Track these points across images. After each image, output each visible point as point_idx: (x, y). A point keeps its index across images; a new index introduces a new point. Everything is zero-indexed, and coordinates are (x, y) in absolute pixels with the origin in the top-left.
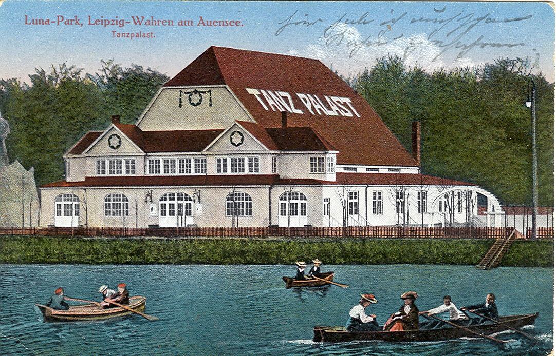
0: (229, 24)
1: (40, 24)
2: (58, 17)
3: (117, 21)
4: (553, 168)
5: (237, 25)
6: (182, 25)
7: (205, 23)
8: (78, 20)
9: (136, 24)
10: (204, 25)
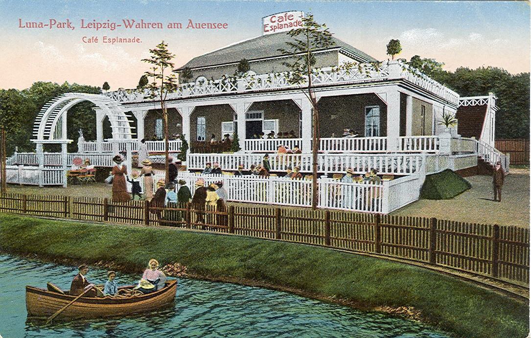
2: (51, 20)
3: (108, 24)
6: (139, 27)
7: (194, 26)
8: (70, 23)
9: (127, 27)
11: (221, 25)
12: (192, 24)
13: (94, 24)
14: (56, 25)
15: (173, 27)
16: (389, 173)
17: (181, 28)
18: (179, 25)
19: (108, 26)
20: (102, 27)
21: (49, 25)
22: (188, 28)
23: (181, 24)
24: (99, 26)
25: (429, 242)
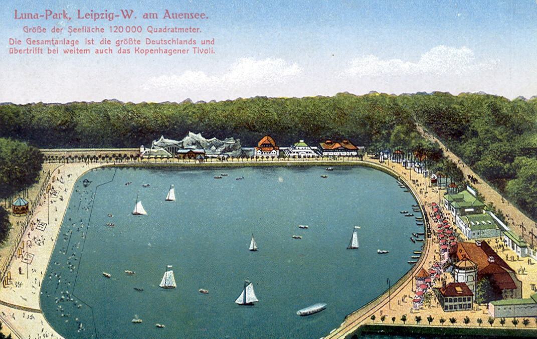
0: (194, 16)
1: (153, 18)
2: (47, 11)
3: (106, 14)
4: (252, 101)
5: (180, 18)
6: (147, 18)
7: (171, 16)
8: (66, 14)
9: (125, 17)
10: (170, 18)
11: (89, 15)
12: (169, 14)
13: (92, 14)
14: (52, 15)
15: (27, 17)
16: (465, 297)
17: (157, 18)
18: (155, 15)
19: (106, 16)
20: (100, 17)
21: (45, 16)
22: (164, 18)
23: (156, 14)
24: (97, 16)
25: (60, 150)
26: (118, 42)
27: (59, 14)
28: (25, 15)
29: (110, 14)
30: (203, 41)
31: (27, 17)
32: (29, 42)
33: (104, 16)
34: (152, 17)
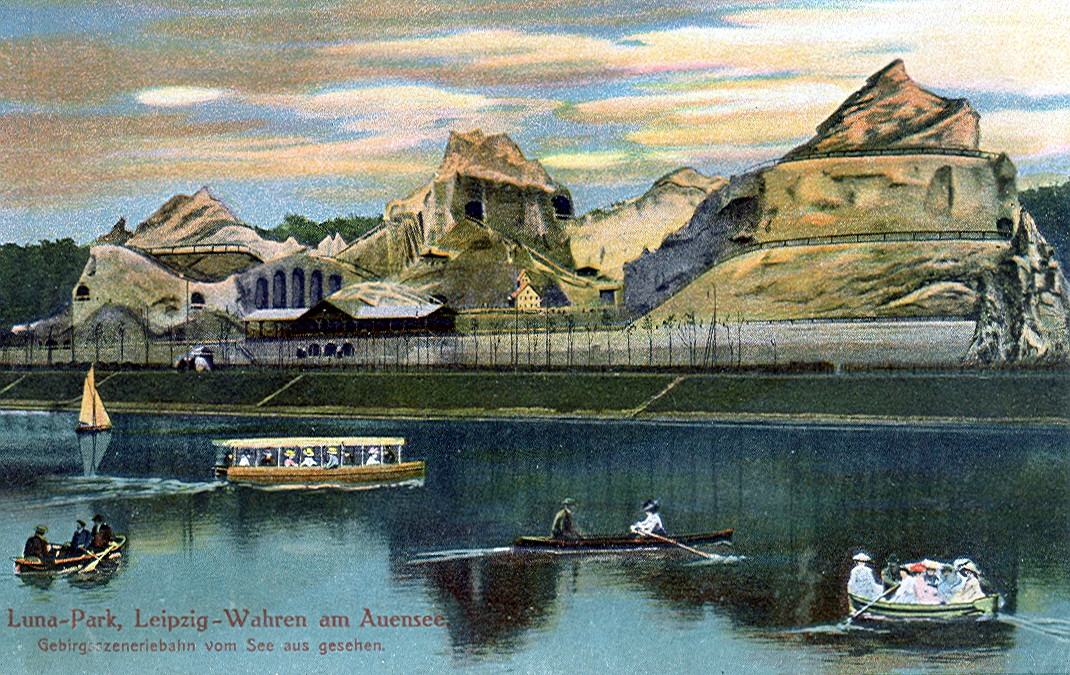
2: (74, 611)
7: (376, 622)
8: (114, 617)
9: (233, 624)
10: (373, 625)
12: (370, 617)
14: (85, 621)
15: (34, 620)
18: (343, 620)
26: (323, 647)
27: (277, 618)
28: (37, 624)
29: (199, 619)
30: (358, 650)
31: (34, 620)
32: (44, 646)
33: (189, 621)
34: (337, 623)
